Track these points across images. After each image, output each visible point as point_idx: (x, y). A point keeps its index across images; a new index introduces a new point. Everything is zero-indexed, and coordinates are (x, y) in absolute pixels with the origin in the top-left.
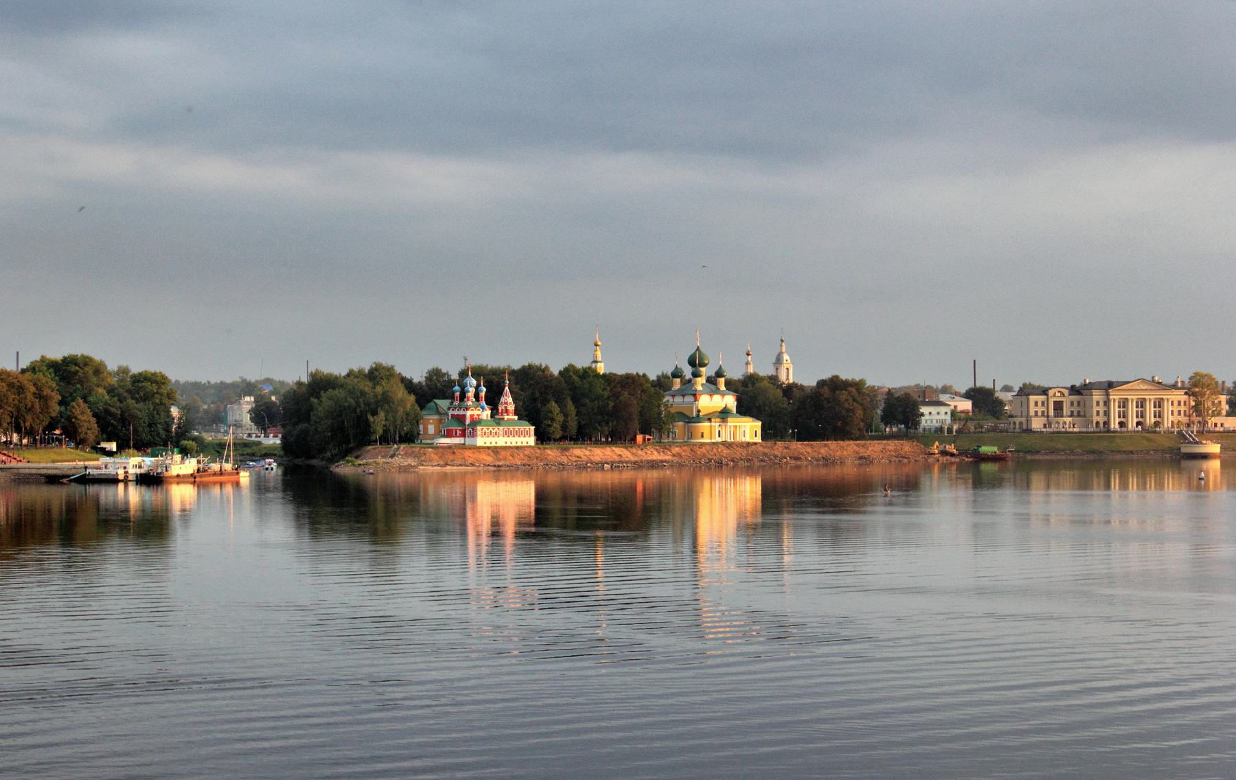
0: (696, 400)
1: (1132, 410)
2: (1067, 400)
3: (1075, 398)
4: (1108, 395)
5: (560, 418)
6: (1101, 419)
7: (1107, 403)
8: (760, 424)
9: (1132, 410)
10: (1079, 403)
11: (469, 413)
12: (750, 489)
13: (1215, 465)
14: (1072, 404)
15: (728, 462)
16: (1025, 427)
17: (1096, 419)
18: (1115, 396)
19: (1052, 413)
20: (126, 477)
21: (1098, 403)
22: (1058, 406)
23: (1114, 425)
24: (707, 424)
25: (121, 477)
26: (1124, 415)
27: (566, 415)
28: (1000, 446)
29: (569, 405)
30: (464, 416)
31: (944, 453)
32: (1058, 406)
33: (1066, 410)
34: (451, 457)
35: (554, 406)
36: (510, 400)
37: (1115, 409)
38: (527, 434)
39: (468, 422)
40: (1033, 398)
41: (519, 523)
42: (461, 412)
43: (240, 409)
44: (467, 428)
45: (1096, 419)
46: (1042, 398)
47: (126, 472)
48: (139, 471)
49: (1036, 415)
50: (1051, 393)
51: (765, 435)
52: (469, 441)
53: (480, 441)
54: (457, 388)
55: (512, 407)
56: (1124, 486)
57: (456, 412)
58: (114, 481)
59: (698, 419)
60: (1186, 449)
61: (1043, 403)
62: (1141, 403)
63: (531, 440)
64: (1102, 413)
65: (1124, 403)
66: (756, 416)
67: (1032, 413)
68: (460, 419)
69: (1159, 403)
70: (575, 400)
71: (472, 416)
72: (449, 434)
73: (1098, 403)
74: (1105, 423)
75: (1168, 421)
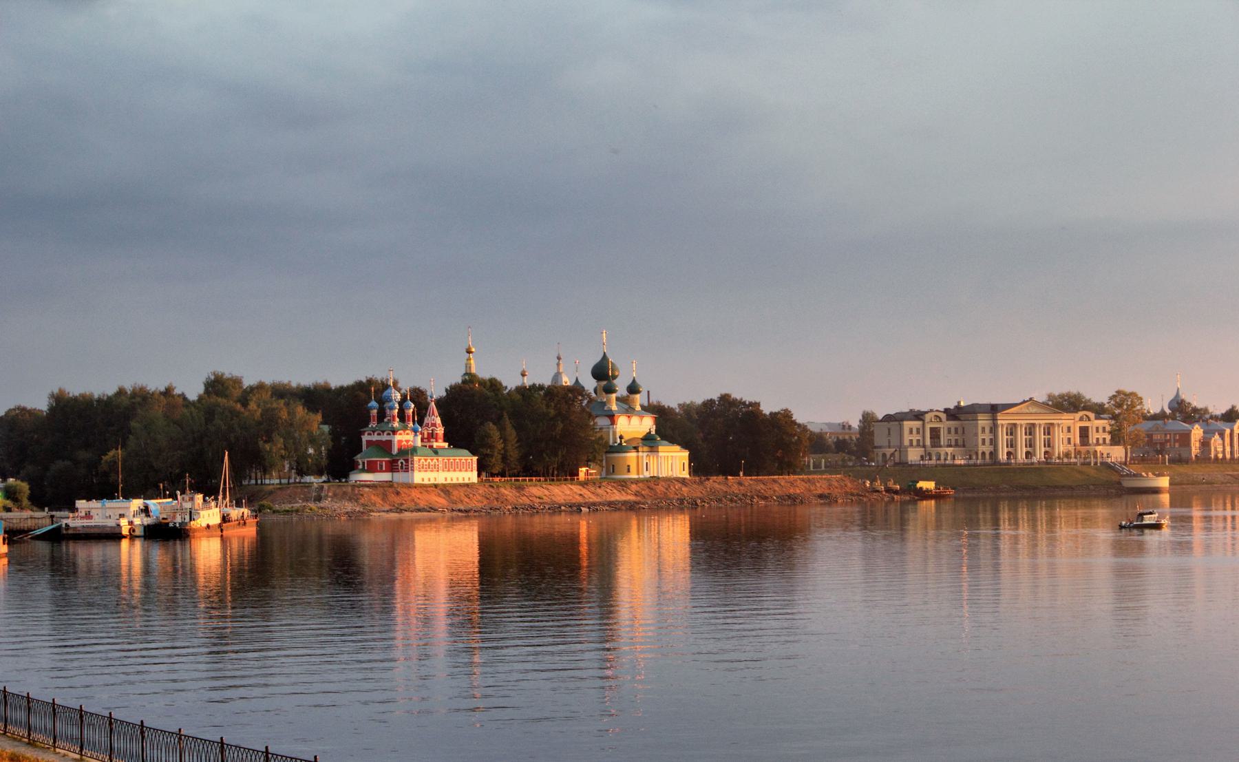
0: (613, 422)
1: (1021, 438)
2: (944, 425)
3: (952, 424)
4: (994, 419)
5: (500, 445)
6: (987, 449)
7: (994, 429)
8: (686, 454)
9: (1021, 438)
10: (956, 429)
11: (397, 438)
12: (675, 533)
13: (1165, 498)
14: (949, 430)
15: (656, 500)
16: (897, 460)
17: (981, 449)
18: (1003, 420)
19: (928, 442)
20: (132, 530)
21: (983, 429)
22: (935, 433)
23: (1002, 456)
24: (633, 455)
25: (125, 531)
26: (1012, 444)
27: (505, 441)
28: (966, 482)
29: (525, 431)
30: (390, 443)
31: (888, 490)
32: (935, 433)
33: (943, 439)
34: (397, 500)
35: (491, 428)
36: (438, 421)
37: (1003, 438)
38: (468, 468)
39: (395, 450)
40: (907, 424)
41: (452, 585)
42: (384, 438)
43: (976, 426)
44: (400, 460)
45: (981, 449)
46: (918, 424)
47: (131, 523)
48: (147, 521)
49: (911, 445)
50: (928, 417)
51: (698, 466)
52: (399, 477)
53: (419, 477)
54: (373, 404)
55: (440, 431)
56: (1015, 522)
57: (375, 438)
58: (114, 536)
59: (620, 449)
60: (1128, 483)
61: (918, 430)
62: (1031, 429)
63: (472, 476)
64: (987, 442)
65: (1012, 429)
66: (685, 445)
67: (906, 443)
68: (386, 447)
69: (1048, 430)
70: (519, 428)
71: (400, 441)
72: (372, 468)
73: (983, 429)
74: (991, 453)
75: (1060, 447)
